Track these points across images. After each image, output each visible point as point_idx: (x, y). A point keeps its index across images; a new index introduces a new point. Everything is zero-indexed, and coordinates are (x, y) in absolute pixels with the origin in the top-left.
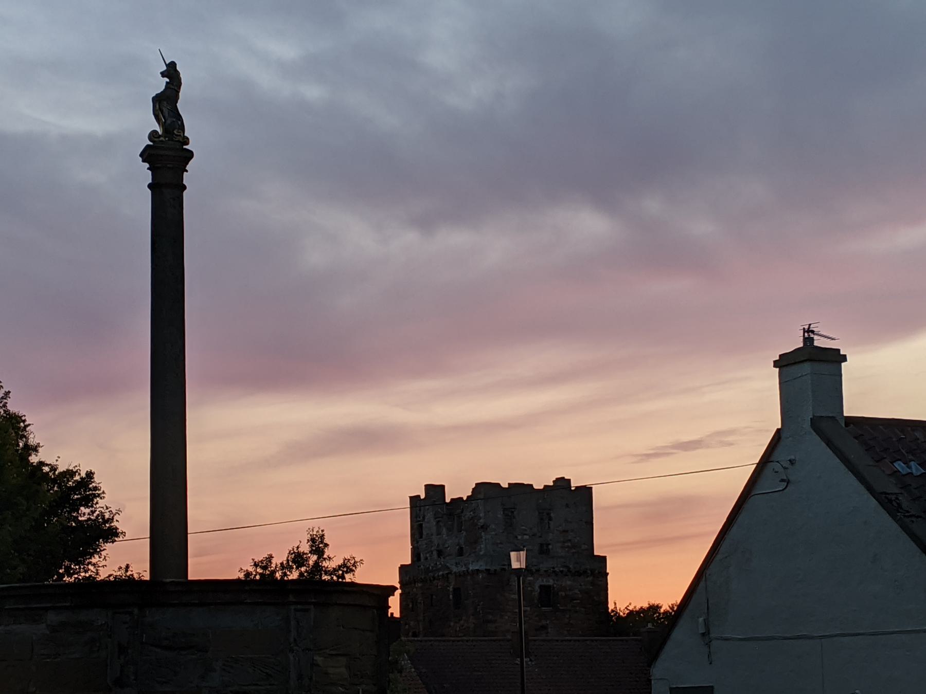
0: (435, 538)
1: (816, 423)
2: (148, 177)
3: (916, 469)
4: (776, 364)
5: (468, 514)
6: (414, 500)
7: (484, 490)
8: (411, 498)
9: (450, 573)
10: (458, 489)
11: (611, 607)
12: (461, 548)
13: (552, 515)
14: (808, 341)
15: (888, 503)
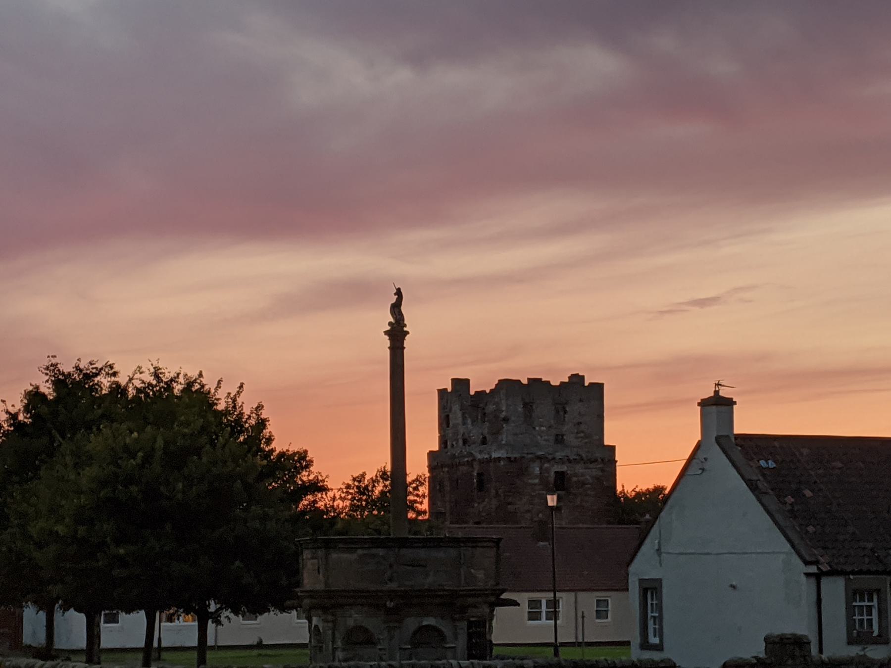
0: (462, 430)
1: (718, 440)
2: (388, 344)
3: (772, 464)
4: (699, 404)
5: (491, 408)
6: (442, 393)
7: (507, 386)
8: (439, 390)
9: (474, 460)
10: (482, 381)
11: (619, 489)
12: (484, 438)
13: (567, 409)
14: (716, 392)
15: (753, 486)
